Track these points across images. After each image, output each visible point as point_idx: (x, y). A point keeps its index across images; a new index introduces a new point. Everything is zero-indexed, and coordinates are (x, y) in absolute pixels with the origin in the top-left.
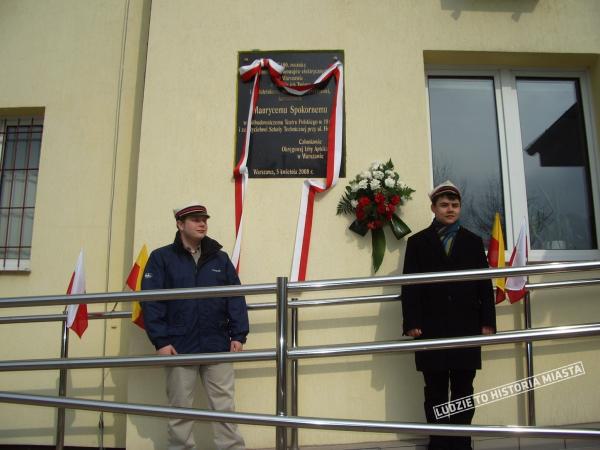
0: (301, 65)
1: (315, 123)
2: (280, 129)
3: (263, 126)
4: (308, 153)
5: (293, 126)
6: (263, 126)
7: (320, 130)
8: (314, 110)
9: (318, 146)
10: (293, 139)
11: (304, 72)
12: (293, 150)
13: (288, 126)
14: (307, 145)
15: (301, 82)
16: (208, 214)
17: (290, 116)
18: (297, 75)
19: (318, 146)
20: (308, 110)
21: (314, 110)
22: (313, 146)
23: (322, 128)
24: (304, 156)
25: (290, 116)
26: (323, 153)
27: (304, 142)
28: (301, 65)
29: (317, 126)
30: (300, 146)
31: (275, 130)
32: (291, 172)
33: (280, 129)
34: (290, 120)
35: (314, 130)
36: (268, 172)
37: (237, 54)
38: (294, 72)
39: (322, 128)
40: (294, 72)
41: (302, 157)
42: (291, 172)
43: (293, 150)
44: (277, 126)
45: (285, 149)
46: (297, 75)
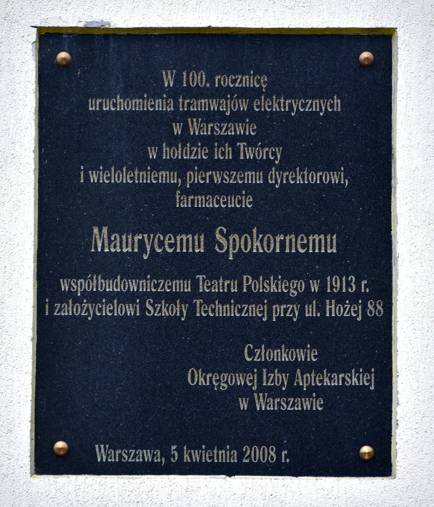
0: (247, 81)
1: (295, 287)
2: (179, 310)
3: (127, 297)
4: (274, 392)
5: (224, 298)
6: (127, 297)
7: (311, 312)
8: (295, 244)
9: (307, 367)
10: (222, 343)
11: (264, 105)
12: (224, 381)
13: (209, 298)
14: (272, 366)
15: (251, 141)
16: (33, 153)
17: (212, 264)
18: (237, 117)
19: (307, 367)
20: (274, 243)
21: (295, 244)
22: (289, 368)
23: (321, 308)
24: (261, 404)
25: (212, 264)
26: (65, 297)
27: (263, 354)
28: (247, 81)
29: (304, 298)
30: (247, 368)
31: (166, 311)
32: (222, 455)
33: (179, 310)
34: (212, 276)
35: (293, 311)
36: (147, 455)
37: (33, 36)
38: (226, 107)
39: (321, 308)
40: (226, 107)
41: (252, 403)
42: (222, 455)
43: (224, 381)
44: (171, 298)
45: (198, 378)
46: (237, 117)
